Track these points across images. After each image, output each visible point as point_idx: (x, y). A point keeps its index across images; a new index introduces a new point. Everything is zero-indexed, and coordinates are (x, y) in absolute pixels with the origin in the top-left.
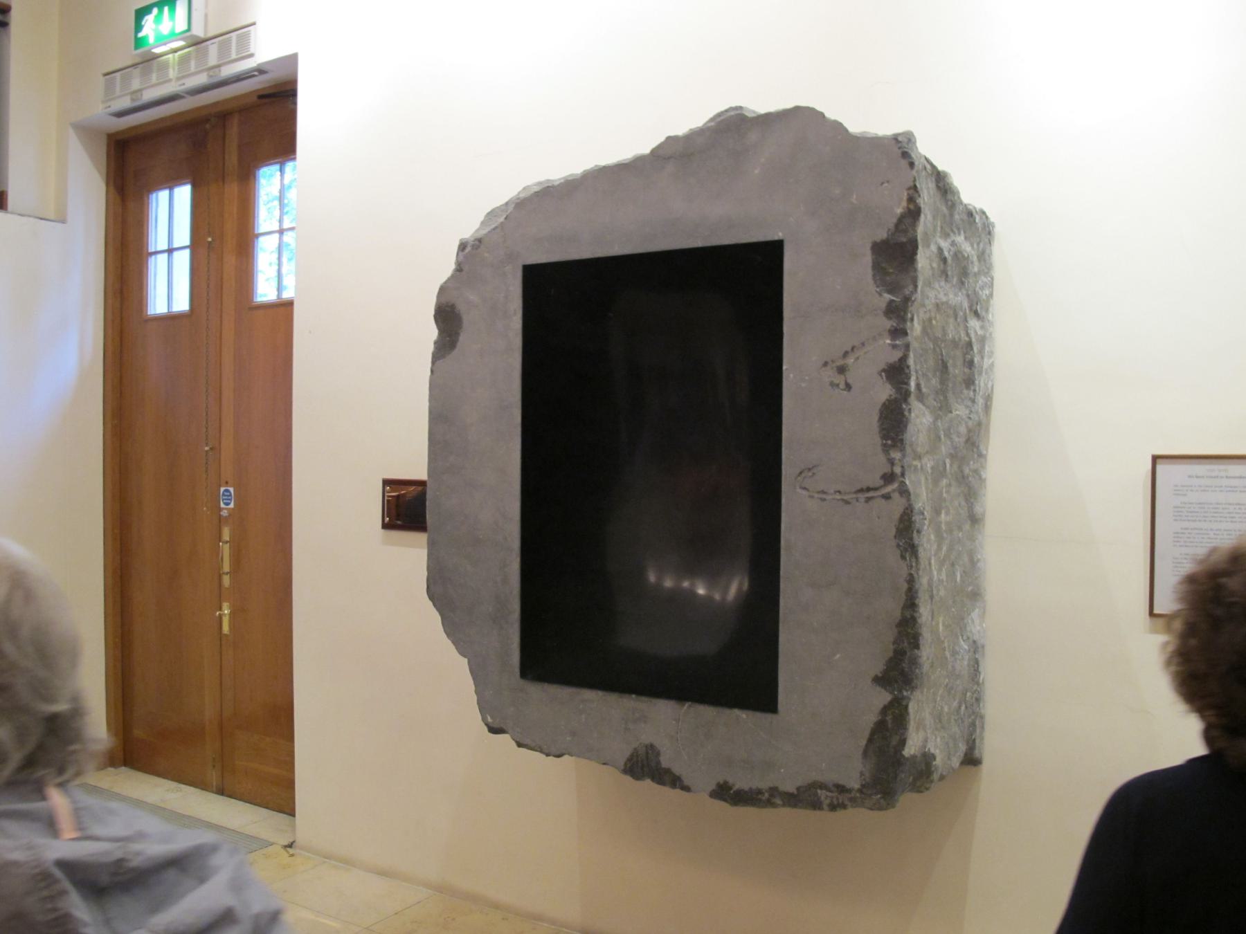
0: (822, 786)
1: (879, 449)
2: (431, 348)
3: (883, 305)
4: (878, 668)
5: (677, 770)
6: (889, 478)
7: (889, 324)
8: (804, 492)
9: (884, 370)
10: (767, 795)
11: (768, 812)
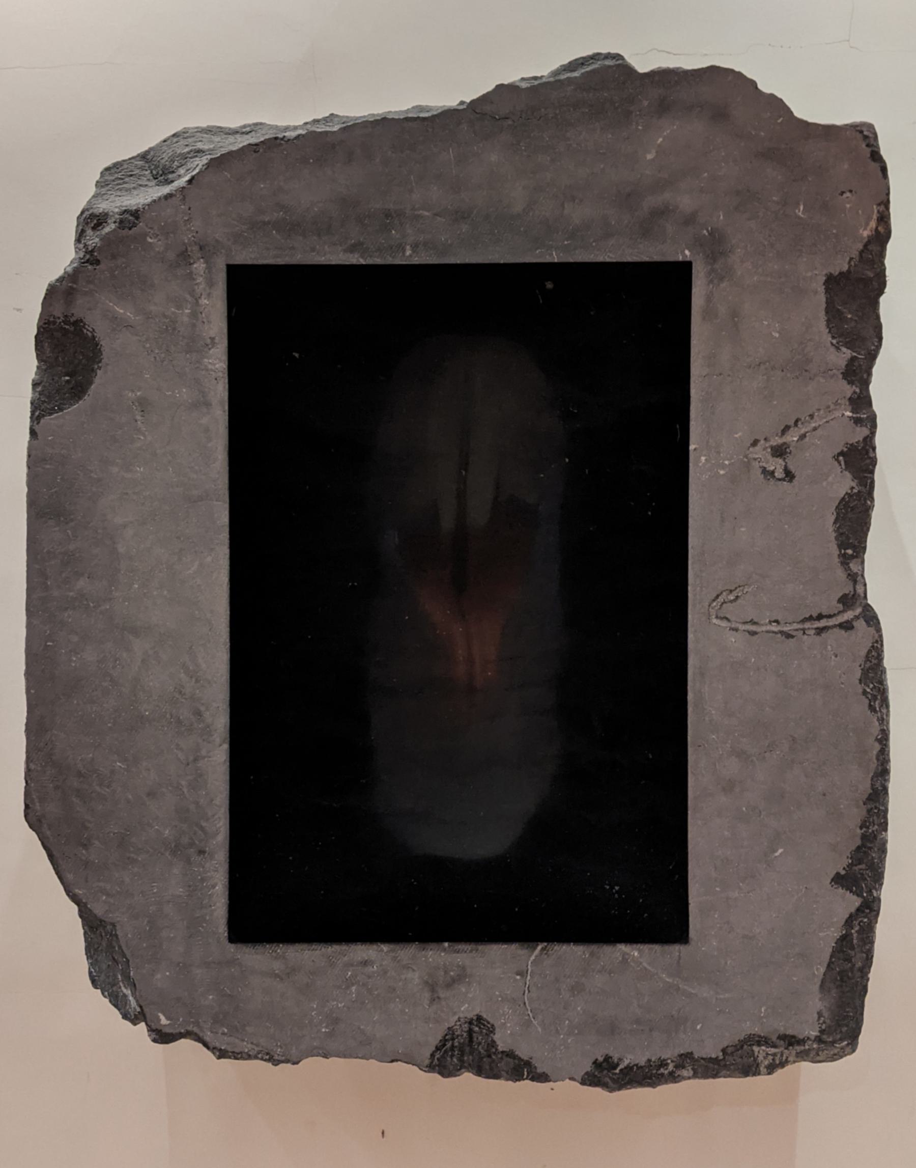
0: (762, 1041)
1: (836, 560)
2: (27, 394)
3: (843, 363)
4: (840, 865)
5: (523, 1053)
6: (848, 601)
7: (849, 390)
8: (724, 624)
9: (841, 453)
10: (671, 1067)
11: (665, 1090)
